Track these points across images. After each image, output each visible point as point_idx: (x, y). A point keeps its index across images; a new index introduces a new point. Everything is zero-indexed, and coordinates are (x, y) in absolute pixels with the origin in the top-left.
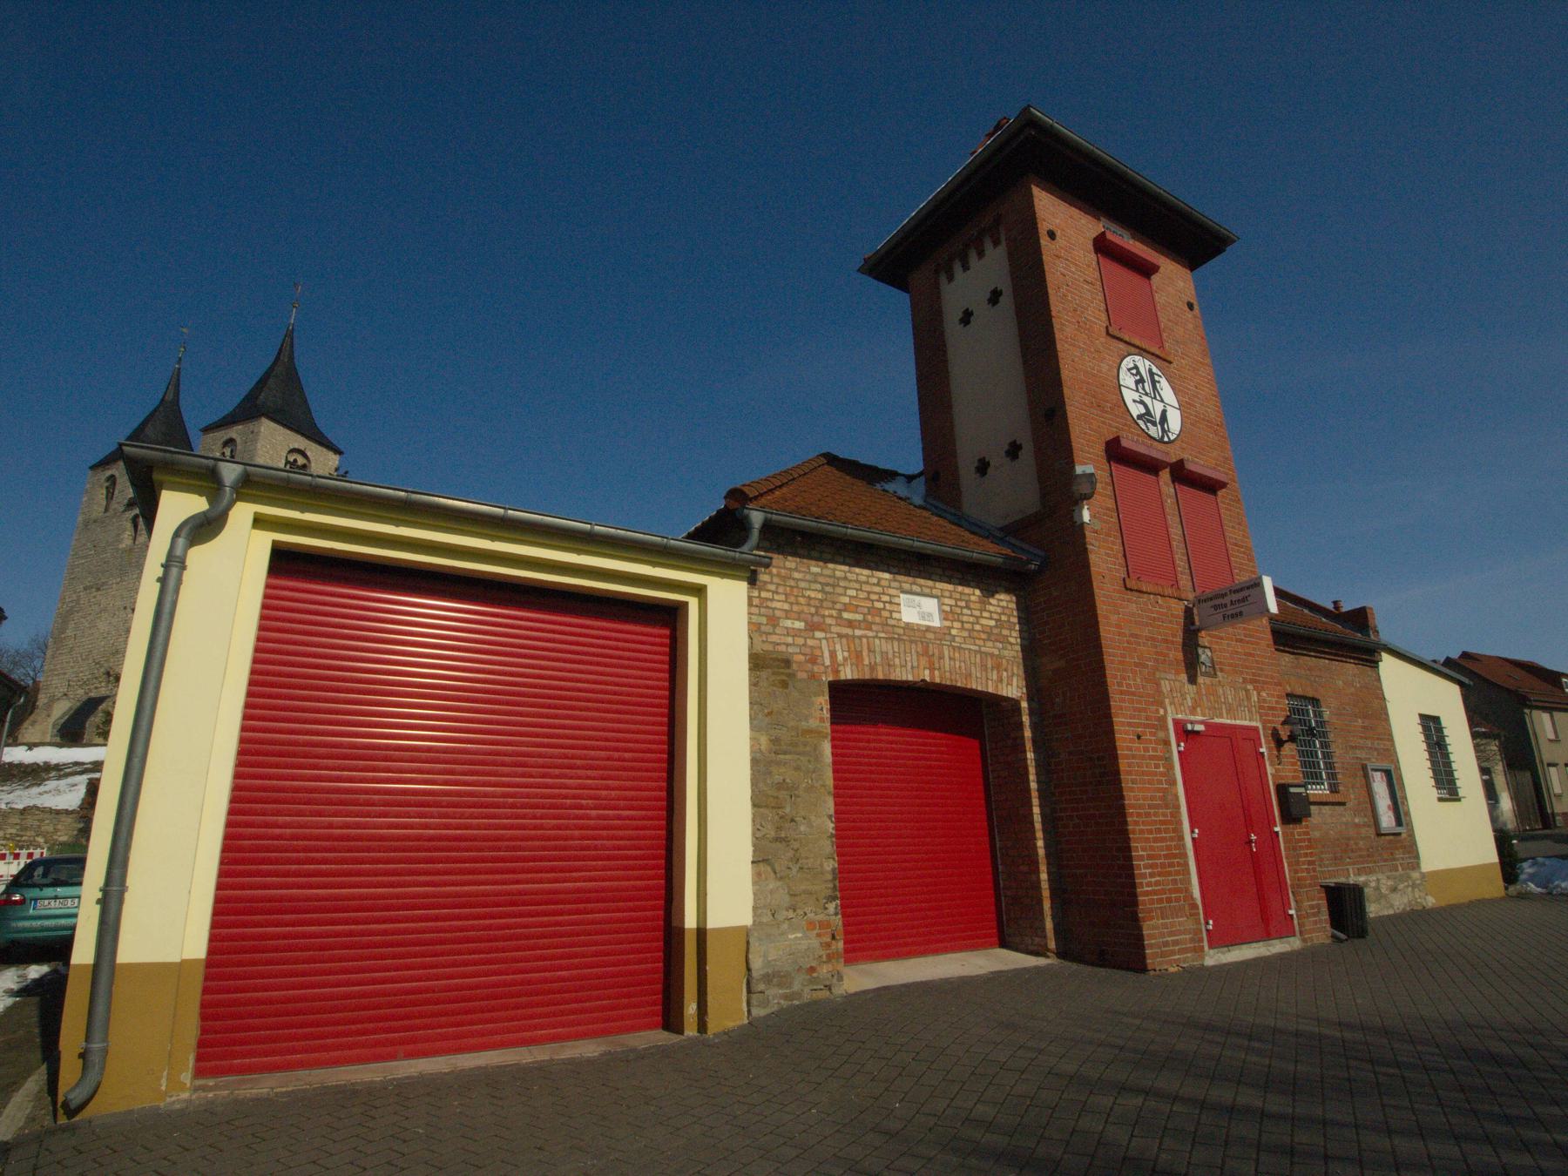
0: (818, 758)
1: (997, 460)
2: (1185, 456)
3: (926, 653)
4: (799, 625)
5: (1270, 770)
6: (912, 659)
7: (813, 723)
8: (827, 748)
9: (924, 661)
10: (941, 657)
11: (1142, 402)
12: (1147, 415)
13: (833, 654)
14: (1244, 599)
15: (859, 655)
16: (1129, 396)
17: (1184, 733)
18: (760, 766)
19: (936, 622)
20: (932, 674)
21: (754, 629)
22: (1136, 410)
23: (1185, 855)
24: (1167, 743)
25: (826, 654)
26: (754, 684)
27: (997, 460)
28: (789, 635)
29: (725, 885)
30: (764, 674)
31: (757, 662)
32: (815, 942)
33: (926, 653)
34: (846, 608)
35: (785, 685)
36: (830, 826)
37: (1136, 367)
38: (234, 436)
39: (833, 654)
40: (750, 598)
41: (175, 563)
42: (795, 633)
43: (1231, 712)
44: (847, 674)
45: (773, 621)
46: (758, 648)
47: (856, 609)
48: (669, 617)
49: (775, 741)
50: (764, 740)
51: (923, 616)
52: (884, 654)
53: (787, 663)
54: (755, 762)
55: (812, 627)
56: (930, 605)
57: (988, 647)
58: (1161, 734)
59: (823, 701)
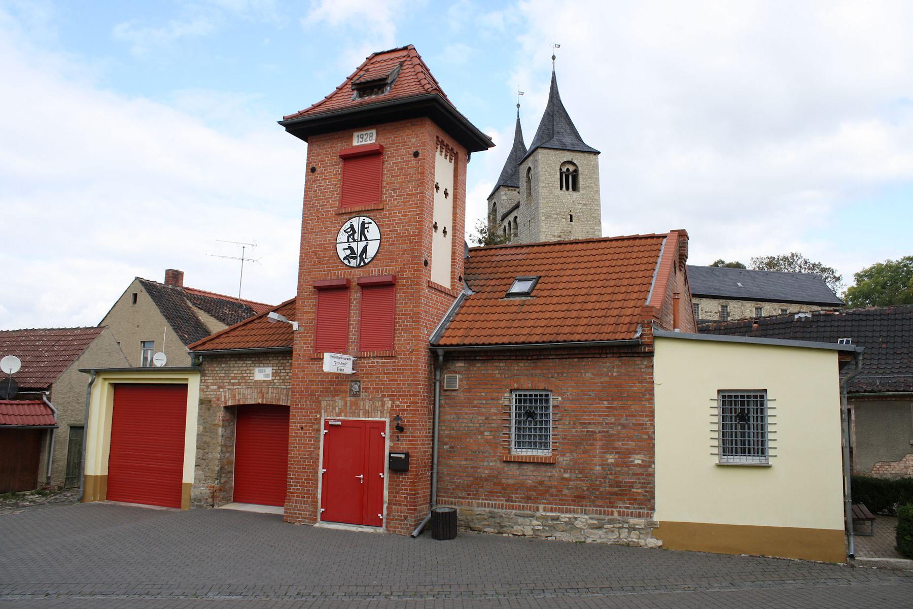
0: (217, 434)
2: (557, 191)
4: (215, 387)
5: (388, 444)
6: (255, 395)
7: (217, 422)
9: (260, 395)
10: (267, 393)
11: (351, 248)
13: (225, 397)
14: (345, 364)
15: (234, 396)
16: (340, 247)
17: (327, 426)
18: (199, 436)
21: (201, 390)
22: (342, 254)
23: (317, 480)
24: (319, 430)
26: (200, 409)
28: (211, 395)
29: (189, 475)
31: (201, 402)
37: (352, 227)
39: (225, 397)
40: (201, 382)
42: (214, 390)
43: (366, 413)
44: (230, 403)
45: (208, 387)
49: (205, 428)
50: (201, 428)
51: (265, 376)
53: (210, 401)
54: (198, 435)
55: (219, 387)
56: (269, 370)
58: (315, 427)
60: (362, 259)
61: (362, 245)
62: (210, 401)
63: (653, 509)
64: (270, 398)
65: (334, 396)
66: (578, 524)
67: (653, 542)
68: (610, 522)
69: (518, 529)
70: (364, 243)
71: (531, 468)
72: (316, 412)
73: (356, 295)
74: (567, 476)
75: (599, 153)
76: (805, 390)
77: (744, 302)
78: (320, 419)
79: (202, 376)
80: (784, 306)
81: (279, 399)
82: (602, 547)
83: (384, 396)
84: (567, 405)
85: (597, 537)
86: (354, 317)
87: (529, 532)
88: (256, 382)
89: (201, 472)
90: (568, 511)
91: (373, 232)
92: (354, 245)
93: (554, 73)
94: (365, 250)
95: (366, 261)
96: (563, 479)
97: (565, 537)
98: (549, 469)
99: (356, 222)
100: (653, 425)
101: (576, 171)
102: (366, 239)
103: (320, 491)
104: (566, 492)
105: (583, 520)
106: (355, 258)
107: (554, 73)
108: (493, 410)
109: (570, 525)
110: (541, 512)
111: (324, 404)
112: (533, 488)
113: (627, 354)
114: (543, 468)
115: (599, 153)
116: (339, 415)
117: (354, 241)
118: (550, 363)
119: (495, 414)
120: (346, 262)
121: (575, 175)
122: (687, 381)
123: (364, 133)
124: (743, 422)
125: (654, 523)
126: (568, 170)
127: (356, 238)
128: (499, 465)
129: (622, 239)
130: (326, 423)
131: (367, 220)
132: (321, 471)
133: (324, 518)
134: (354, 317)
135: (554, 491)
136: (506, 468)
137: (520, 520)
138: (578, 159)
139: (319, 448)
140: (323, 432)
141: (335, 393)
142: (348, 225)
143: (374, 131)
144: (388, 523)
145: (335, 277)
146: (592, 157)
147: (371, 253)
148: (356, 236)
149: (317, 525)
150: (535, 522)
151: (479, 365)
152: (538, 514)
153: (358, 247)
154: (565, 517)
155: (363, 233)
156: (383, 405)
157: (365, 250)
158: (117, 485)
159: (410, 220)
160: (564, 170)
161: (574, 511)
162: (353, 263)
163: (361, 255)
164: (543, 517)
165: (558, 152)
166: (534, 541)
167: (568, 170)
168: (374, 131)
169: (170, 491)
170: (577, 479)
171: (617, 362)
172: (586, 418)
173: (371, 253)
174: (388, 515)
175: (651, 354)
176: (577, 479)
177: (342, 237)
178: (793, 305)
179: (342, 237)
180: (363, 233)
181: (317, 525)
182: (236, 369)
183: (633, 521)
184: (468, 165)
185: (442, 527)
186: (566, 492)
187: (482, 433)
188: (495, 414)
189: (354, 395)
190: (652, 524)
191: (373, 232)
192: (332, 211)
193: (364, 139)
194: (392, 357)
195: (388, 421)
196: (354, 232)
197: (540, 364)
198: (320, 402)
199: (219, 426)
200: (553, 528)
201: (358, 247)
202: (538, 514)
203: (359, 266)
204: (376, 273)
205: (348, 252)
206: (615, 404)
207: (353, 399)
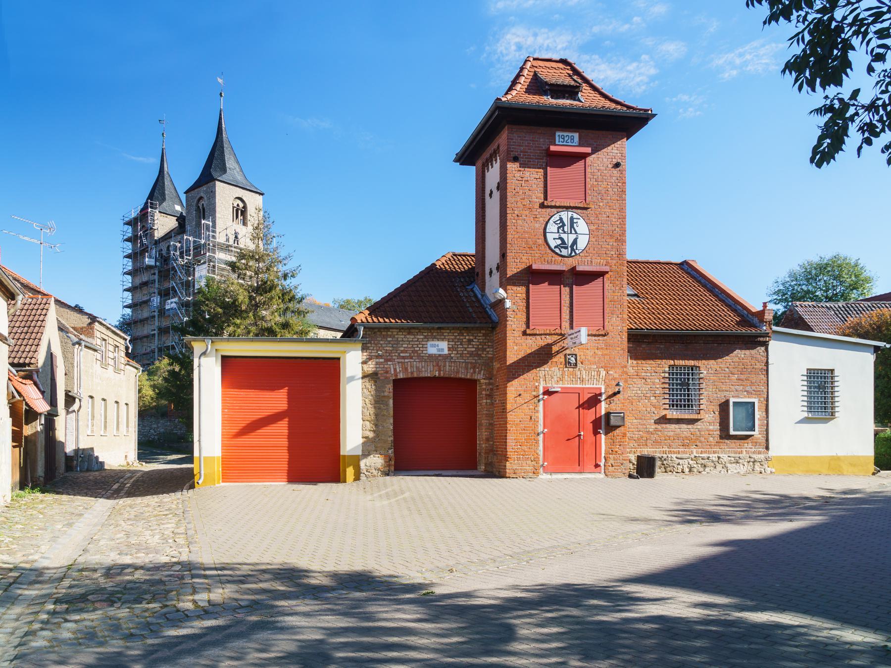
0: (387, 405)
3: (437, 365)
7: (386, 394)
8: (391, 401)
9: (436, 368)
11: (561, 238)
13: (395, 370)
15: (406, 369)
19: (446, 352)
20: (439, 374)
22: (553, 244)
33: (437, 365)
34: (402, 352)
36: (392, 427)
37: (561, 219)
38: (202, 195)
39: (395, 370)
44: (401, 376)
55: (387, 360)
57: (471, 360)
60: (572, 250)
61: (572, 237)
64: (448, 370)
70: (574, 236)
74: (711, 427)
81: (458, 372)
88: (430, 356)
91: (582, 227)
92: (564, 236)
94: (575, 242)
95: (577, 252)
99: (565, 216)
101: (245, 207)
102: (576, 233)
103: (541, 447)
106: (566, 248)
117: (565, 232)
120: (557, 250)
124: (821, 390)
131: (575, 216)
142: (556, 217)
143: (576, 136)
147: (582, 243)
148: (566, 228)
154: (714, 457)
155: (572, 226)
157: (575, 242)
160: (235, 205)
162: (564, 252)
163: (572, 246)
168: (576, 136)
177: (552, 227)
180: (572, 226)
184: (498, 180)
191: (582, 227)
194: (604, 335)
199: (388, 397)
205: (559, 242)
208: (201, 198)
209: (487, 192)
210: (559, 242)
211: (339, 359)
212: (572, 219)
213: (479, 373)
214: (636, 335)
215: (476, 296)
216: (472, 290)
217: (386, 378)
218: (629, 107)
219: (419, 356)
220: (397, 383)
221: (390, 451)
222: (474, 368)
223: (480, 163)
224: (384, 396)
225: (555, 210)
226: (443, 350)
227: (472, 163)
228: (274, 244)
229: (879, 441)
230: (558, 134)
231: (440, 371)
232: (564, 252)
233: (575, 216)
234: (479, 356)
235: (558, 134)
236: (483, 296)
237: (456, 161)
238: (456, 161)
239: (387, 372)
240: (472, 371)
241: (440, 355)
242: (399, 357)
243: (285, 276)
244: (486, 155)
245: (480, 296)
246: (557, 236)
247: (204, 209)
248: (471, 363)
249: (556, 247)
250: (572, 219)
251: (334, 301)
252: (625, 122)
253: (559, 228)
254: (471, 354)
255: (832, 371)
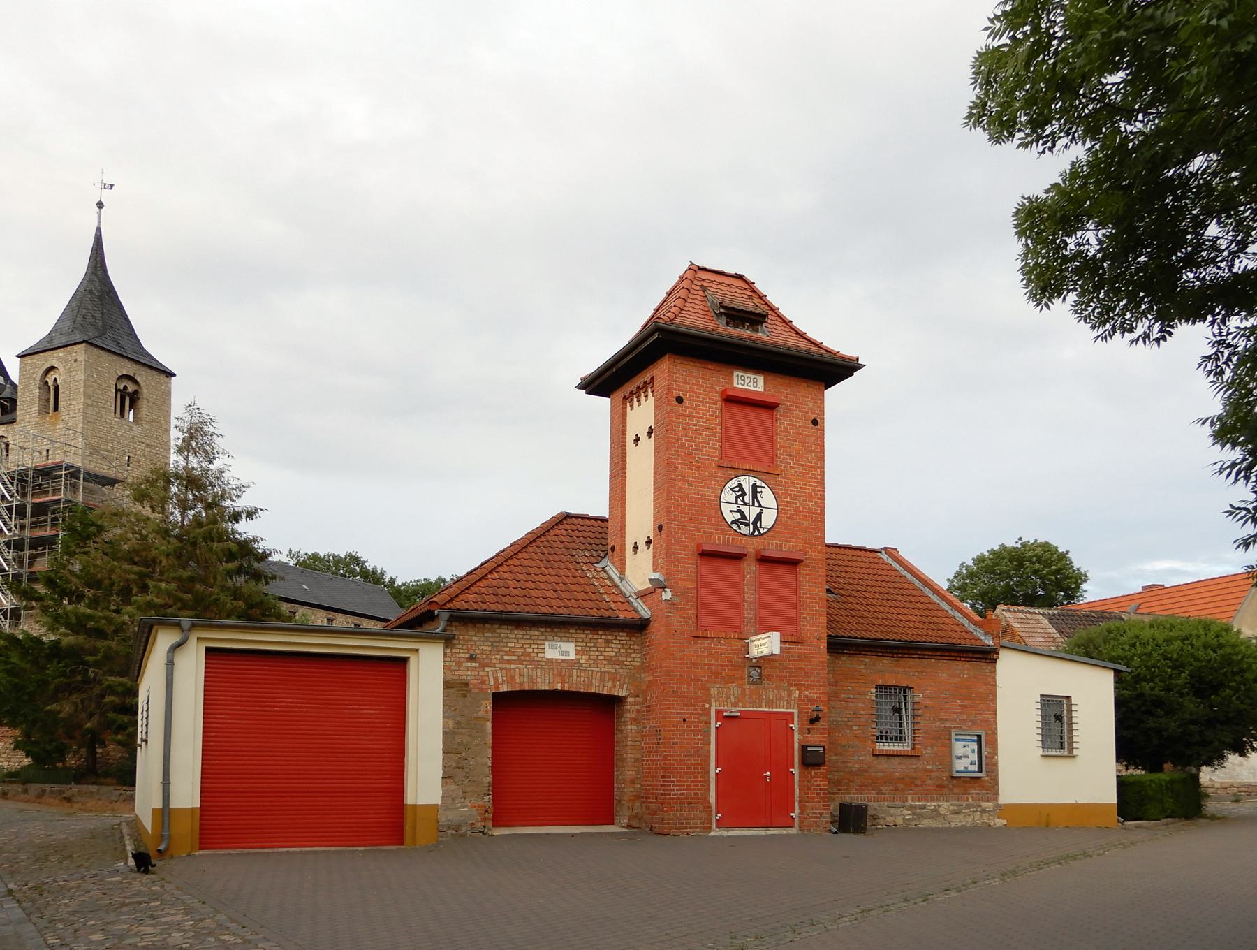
1: (642, 546)
3: (560, 674)
5: (797, 736)
7: (481, 714)
8: (489, 725)
10: (571, 676)
11: (739, 511)
12: (743, 519)
13: (496, 679)
15: (513, 679)
16: (726, 508)
19: (572, 656)
20: (563, 685)
22: (730, 518)
24: (708, 723)
25: (491, 679)
27: (642, 546)
28: (468, 672)
30: (452, 691)
32: (475, 813)
33: (560, 674)
34: (507, 653)
35: (465, 696)
36: (489, 763)
37: (740, 486)
38: (55, 363)
39: (496, 679)
40: (445, 654)
41: (170, 664)
43: (770, 703)
44: (504, 688)
46: (449, 678)
47: (513, 654)
48: (400, 665)
49: (458, 723)
50: (451, 723)
52: (530, 677)
53: (467, 685)
54: (444, 733)
57: (609, 669)
58: (704, 718)
59: (487, 705)
60: (755, 527)
61: (755, 511)
62: (467, 685)
63: (997, 793)
64: (575, 683)
65: (726, 683)
66: (943, 811)
67: (1001, 822)
68: (968, 806)
69: (890, 820)
70: (758, 510)
71: (898, 760)
72: (703, 701)
73: (750, 568)
74: (929, 767)
75: (174, 375)
76: (1093, 694)
77: (316, 610)
78: (709, 709)
79: (446, 647)
80: (358, 620)
82: (961, 830)
83: (790, 685)
84: (927, 702)
85: (957, 821)
86: (749, 595)
87: (899, 822)
89: (453, 787)
90: (933, 800)
92: (745, 509)
93: (99, 230)
94: (759, 517)
96: (927, 770)
97: (932, 823)
98: (914, 760)
99: (747, 482)
100: (995, 722)
104: (929, 782)
105: (945, 807)
106: (747, 524)
107: (99, 230)
108: (861, 705)
109: (936, 813)
110: (910, 803)
111: (714, 691)
112: (901, 779)
113: (979, 660)
114: (909, 761)
115: (174, 375)
116: (735, 705)
118: (911, 662)
119: (863, 709)
121: (134, 399)
122: (1021, 682)
123: (746, 375)
124: (1056, 718)
125: (1000, 806)
126: (125, 387)
127: (746, 499)
128: (869, 758)
129: (850, 548)
130: (719, 712)
131: (759, 483)
132: (713, 770)
133: (720, 824)
134: (749, 595)
135: (918, 782)
136: (875, 761)
137: (892, 811)
138: (143, 376)
139: (709, 744)
140: (714, 725)
141: (729, 679)
142: (734, 483)
144: (801, 822)
145: (719, 542)
146: (163, 378)
147: (768, 520)
149: (712, 834)
150: (905, 812)
151: (844, 658)
152: (907, 804)
153: (752, 513)
154: (931, 805)
155: (755, 497)
156: (789, 695)
157: (759, 517)
158: (229, 815)
159: (810, 495)
161: (938, 800)
162: (744, 530)
163: (755, 523)
164: (912, 808)
165: (114, 357)
166: (907, 828)
167: (125, 387)
169: (381, 816)
170: (939, 770)
171: (967, 665)
172: (943, 715)
173: (768, 520)
174: (802, 813)
175: (995, 661)
176: (939, 770)
177: (728, 496)
178: (367, 621)
179: (728, 496)
180: (755, 497)
181: (712, 834)
182: (513, 641)
183: (984, 805)
185: (852, 820)
186: (929, 782)
187: (850, 728)
188: (863, 709)
189: (753, 683)
190: (998, 807)
192: (713, 461)
193: (751, 383)
195: (796, 711)
196: (744, 494)
197: (902, 661)
198: (708, 690)
200: (921, 816)
201: (752, 513)
202: (907, 804)
203: (752, 535)
204: (773, 548)
205: (738, 516)
206: (966, 702)
207: (752, 687)
208: (52, 368)
209: (630, 438)
210: (738, 516)
211: (404, 661)
212: (755, 486)
213: (621, 687)
214: (836, 644)
215: (610, 578)
216: (604, 570)
217: (482, 690)
218: (813, 343)
219: (532, 661)
220: (500, 700)
221: (487, 798)
222: (614, 680)
223: (619, 395)
224: (477, 718)
225: (732, 472)
226: (567, 653)
227: (606, 394)
228: (217, 464)
229: (1123, 785)
230: (736, 373)
231: (563, 683)
232: (744, 530)
233: (759, 483)
234: (621, 664)
235: (736, 373)
236: (622, 579)
237: (580, 387)
238: (580, 387)
239: (483, 682)
240: (610, 684)
241: (563, 661)
242: (502, 660)
243: (236, 517)
244: (631, 386)
245: (617, 580)
246: (734, 507)
247: (57, 389)
248: (609, 673)
249: (733, 522)
250: (755, 486)
251: (291, 554)
252: (835, 369)
253: (737, 497)
254: (610, 661)
255: (1068, 698)
